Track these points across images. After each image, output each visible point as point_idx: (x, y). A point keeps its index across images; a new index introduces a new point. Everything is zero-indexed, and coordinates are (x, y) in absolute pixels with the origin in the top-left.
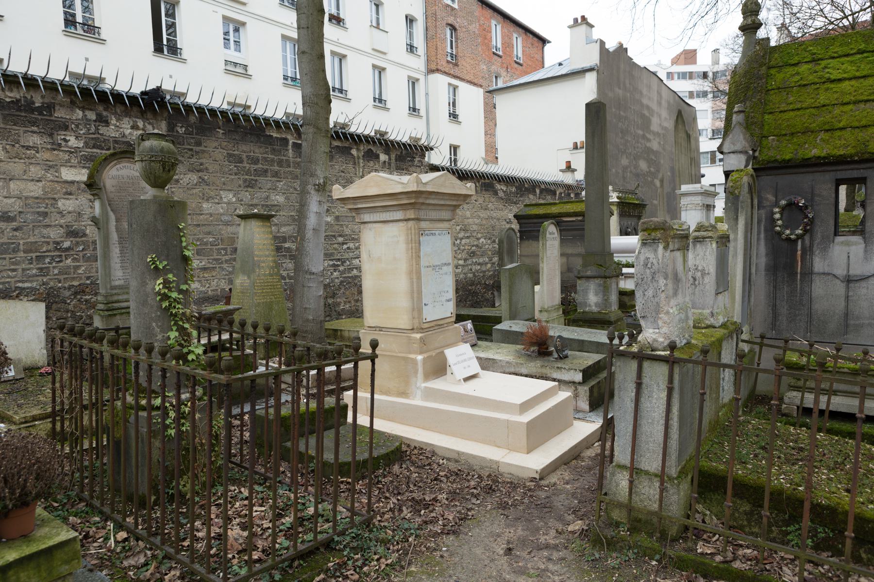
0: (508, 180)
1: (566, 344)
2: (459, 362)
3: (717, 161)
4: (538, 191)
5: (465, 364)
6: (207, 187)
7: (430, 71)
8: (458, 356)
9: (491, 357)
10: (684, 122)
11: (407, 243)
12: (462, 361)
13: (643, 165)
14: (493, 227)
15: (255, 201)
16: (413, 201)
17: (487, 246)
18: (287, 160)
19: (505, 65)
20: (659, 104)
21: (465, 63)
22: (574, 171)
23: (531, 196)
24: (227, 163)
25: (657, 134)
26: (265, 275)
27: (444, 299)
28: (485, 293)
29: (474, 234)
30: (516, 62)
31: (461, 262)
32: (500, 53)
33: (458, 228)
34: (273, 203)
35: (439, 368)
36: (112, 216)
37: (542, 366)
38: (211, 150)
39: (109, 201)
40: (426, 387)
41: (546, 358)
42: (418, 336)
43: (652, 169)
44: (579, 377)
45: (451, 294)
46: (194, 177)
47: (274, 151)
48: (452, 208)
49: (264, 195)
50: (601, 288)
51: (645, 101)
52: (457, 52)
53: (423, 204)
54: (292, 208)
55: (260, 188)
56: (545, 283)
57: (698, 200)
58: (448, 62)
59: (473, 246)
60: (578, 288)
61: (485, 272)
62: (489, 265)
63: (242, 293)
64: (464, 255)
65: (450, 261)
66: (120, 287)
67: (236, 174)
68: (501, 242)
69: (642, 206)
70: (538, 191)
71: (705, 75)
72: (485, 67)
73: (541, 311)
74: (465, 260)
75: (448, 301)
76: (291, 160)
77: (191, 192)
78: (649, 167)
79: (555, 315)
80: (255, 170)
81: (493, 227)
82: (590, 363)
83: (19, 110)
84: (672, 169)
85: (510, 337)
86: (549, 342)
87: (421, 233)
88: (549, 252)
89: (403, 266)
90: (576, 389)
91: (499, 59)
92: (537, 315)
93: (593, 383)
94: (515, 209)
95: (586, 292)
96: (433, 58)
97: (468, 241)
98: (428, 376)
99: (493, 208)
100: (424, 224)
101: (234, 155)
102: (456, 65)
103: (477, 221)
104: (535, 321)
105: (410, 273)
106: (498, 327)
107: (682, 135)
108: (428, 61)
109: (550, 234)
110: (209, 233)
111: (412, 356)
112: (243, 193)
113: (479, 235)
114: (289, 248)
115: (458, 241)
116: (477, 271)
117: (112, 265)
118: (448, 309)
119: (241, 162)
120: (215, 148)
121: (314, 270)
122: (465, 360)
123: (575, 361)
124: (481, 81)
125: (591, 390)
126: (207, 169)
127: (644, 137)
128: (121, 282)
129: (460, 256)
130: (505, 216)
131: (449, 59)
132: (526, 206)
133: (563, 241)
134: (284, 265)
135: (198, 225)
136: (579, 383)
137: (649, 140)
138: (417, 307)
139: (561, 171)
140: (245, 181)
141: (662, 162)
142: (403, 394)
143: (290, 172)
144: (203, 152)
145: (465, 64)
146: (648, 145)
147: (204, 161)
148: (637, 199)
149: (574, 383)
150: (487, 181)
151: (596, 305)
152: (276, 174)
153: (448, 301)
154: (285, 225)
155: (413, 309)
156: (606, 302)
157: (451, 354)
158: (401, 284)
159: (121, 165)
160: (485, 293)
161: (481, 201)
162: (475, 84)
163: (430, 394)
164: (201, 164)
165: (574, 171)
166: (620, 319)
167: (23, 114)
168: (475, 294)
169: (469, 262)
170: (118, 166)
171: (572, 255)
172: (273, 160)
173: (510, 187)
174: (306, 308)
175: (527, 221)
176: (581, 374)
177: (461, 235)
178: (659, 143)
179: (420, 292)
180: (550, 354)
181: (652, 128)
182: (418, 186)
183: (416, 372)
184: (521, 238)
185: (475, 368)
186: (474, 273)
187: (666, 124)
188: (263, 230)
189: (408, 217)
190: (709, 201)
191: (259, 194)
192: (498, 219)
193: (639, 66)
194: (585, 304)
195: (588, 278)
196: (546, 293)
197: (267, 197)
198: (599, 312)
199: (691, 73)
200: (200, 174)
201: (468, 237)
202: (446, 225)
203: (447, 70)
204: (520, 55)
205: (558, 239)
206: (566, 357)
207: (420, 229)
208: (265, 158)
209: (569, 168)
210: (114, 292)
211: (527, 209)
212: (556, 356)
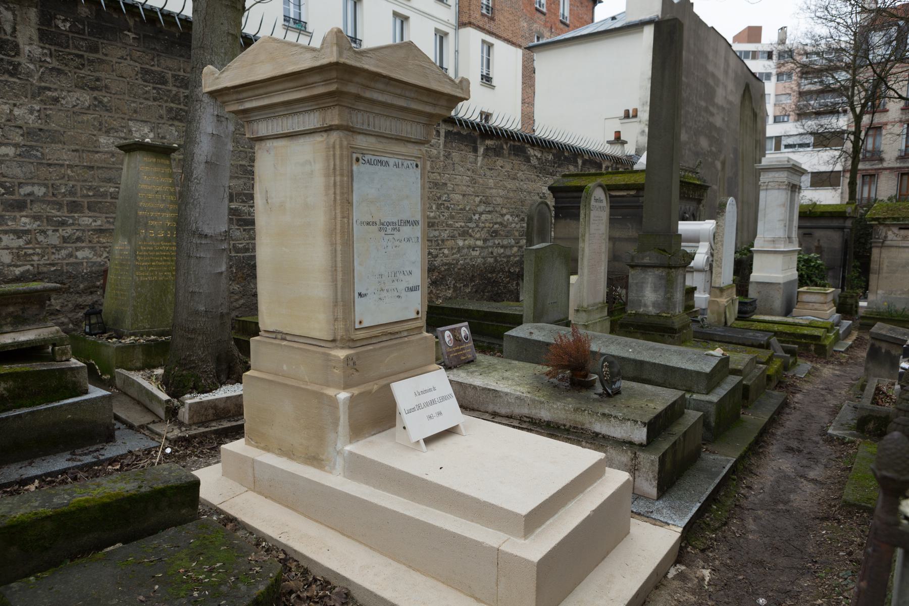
0: (546, 145)
1: (621, 369)
2: (419, 407)
3: (783, 147)
4: (580, 162)
5: (432, 410)
6: (107, 114)
7: (461, 24)
8: (418, 394)
9: (492, 385)
10: (751, 97)
11: (327, 176)
12: (427, 404)
13: (704, 143)
14: (523, 202)
16: (333, 87)
17: (513, 225)
19: (549, 24)
20: (726, 72)
21: (503, 18)
22: (624, 143)
23: (571, 168)
24: (140, 82)
25: (721, 108)
26: (156, 239)
27: (402, 286)
28: (509, 282)
29: (498, 209)
30: (562, 22)
31: (479, 243)
32: (544, 10)
33: (477, 199)
35: (380, 416)
37: (576, 410)
38: (115, 60)
40: (351, 453)
41: (584, 393)
42: (342, 354)
43: (714, 149)
44: (640, 435)
45: (417, 276)
46: (86, 98)
48: (424, 120)
50: (663, 282)
51: (710, 68)
52: (494, 4)
53: (358, 98)
54: (243, 155)
56: (586, 271)
57: (783, 176)
58: (483, 15)
59: (496, 223)
60: (630, 280)
61: (509, 257)
62: (515, 249)
63: (121, 265)
64: (484, 234)
65: (418, 217)
67: (155, 100)
68: (530, 218)
69: (703, 188)
70: (580, 162)
71: (770, 55)
72: (525, 24)
73: (577, 311)
74: (485, 240)
75: (412, 289)
77: (80, 119)
78: (710, 146)
79: (597, 316)
81: (523, 202)
82: (660, 408)
84: (735, 151)
85: (530, 351)
86: (590, 366)
87: (355, 156)
88: (593, 227)
89: (320, 219)
90: (635, 457)
91: (543, 17)
92: (572, 317)
93: (665, 446)
94: (550, 182)
95: (641, 286)
96: (466, 10)
97: (489, 216)
98: (358, 431)
99: (523, 178)
100: (361, 141)
101: (152, 72)
102: (492, 19)
103: (502, 192)
104: (568, 324)
105: (331, 232)
106: (513, 332)
107: (748, 113)
108: (460, 13)
109: (596, 200)
110: (109, 180)
111: (330, 392)
112: (166, 127)
113: (504, 211)
115: (477, 217)
116: (500, 255)
118: (412, 306)
119: (165, 83)
120: (122, 58)
121: (207, 230)
122: (433, 402)
123: (633, 403)
124: (520, 41)
125: (662, 461)
126: (106, 87)
127: (706, 110)
129: (478, 236)
130: (539, 189)
131: (484, 11)
132: (565, 176)
133: (612, 221)
135: (91, 168)
136: (641, 445)
137: (712, 114)
138: (344, 298)
139: (609, 142)
140: (170, 110)
141: (725, 141)
142: (315, 460)
144: (102, 61)
145: (502, 18)
146: (711, 119)
147: (102, 75)
148: (698, 179)
149: (631, 443)
150: (517, 143)
151: (655, 304)
153: (412, 289)
155: (335, 304)
156: (668, 301)
157: (404, 392)
158: (315, 254)
160: (509, 282)
161: (508, 167)
162: (513, 44)
163: (361, 469)
164: (98, 79)
165: (624, 143)
166: (686, 326)
168: (495, 283)
169: (490, 243)
171: (620, 239)
173: (546, 154)
174: (193, 293)
175: (564, 195)
176: (645, 430)
177: (481, 208)
178: (723, 119)
179: (349, 271)
180: (590, 385)
181: (716, 101)
182: (340, 53)
183: (336, 423)
184: (557, 217)
185: (452, 414)
186: (495, 258)
187: (731, 98)
188: (155, 169)
189: (329, 122)
190: (794, 180)
192: (530, 193)
193: (706, 25)
194: (639, 303)
195: (645, 267)
196: (587, 286)
198: (658, 316)
199: (754, 53)
200: (96, 93)
201: (490, 212)
202: (413, 150)
203: (481, 24)
204: (567, 14)
205: (608, 210)
206: (618, 392)
207: (353, 149)
209: (618, 139)
211: (565, 180)
212: (600, 390)
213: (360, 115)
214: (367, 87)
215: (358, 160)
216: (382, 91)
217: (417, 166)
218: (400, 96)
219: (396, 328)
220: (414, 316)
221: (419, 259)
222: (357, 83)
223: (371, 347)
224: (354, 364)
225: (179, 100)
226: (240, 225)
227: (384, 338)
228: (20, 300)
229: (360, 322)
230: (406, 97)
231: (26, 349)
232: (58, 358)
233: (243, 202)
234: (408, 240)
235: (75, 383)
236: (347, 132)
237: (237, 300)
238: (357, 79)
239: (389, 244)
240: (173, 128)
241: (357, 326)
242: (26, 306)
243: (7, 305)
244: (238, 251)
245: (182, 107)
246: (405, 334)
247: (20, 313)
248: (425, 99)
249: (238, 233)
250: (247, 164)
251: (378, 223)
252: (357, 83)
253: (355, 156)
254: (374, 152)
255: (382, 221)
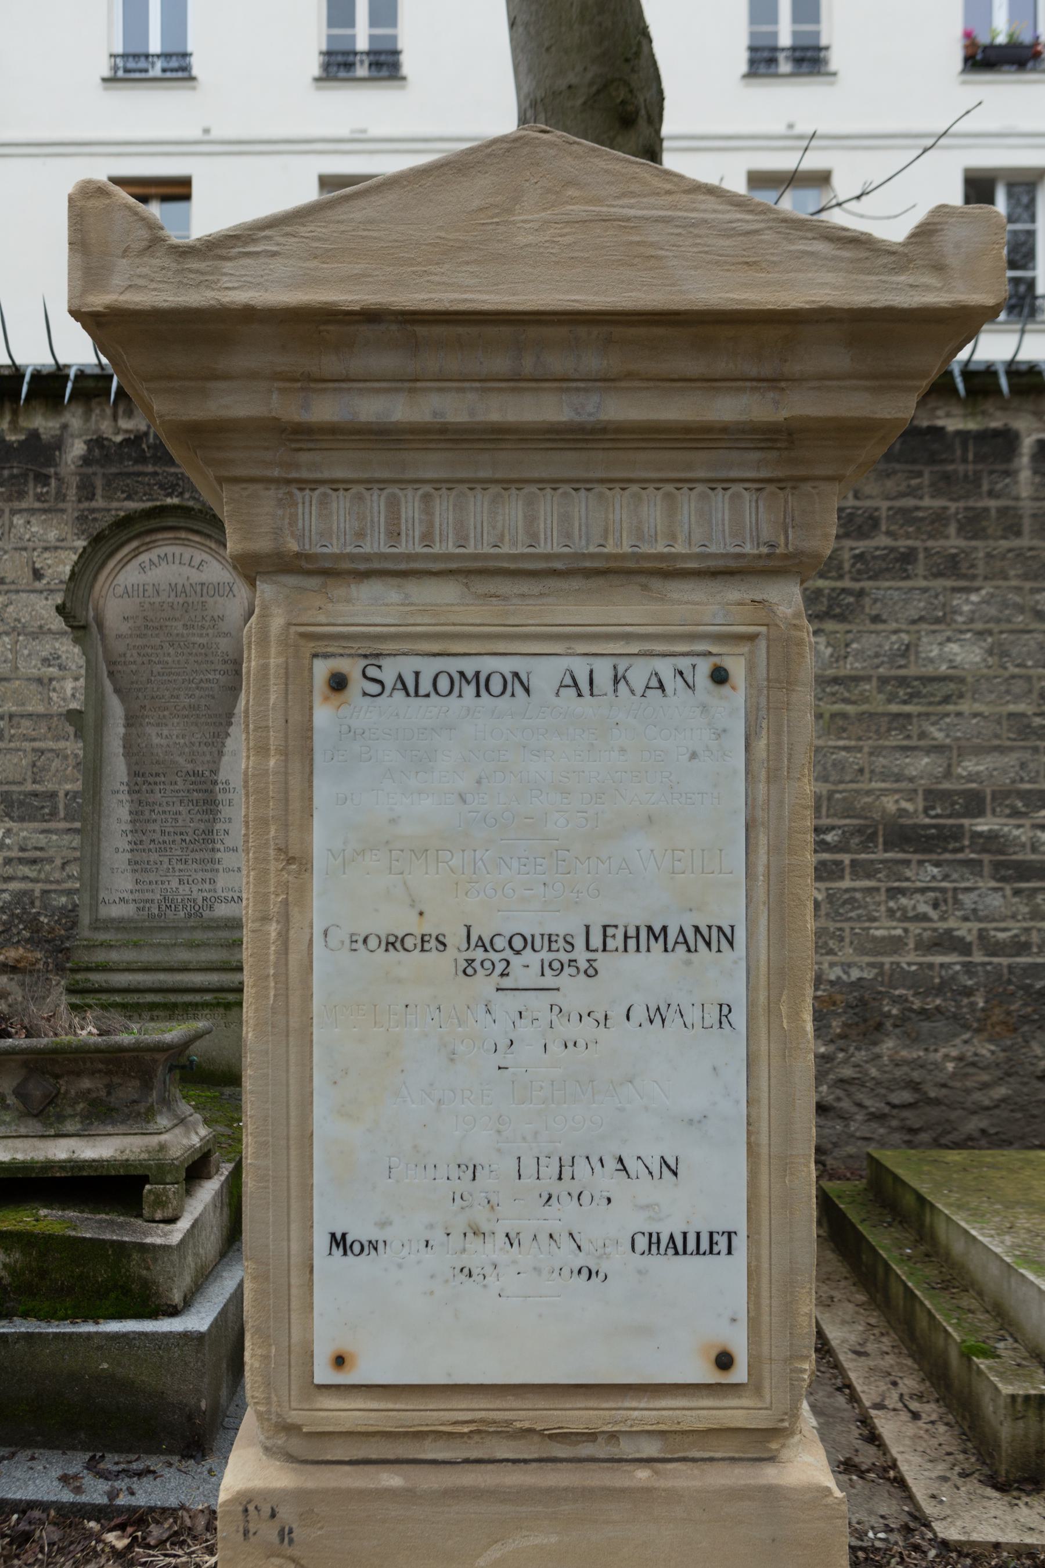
15: (850, 667)
18: (1003, 511)
34: (929, 670)
36: (116, 708)
39: (110, 663)
47: (945, 484)
48: (749, 464)
49: (892, 643)
55: (876, 619)
65: (730, 909)
66: (120, 925)
76: (1027, 507)
80: (860, 557)
83: (142, 459)
114: (992, 837)
117: (106, 855)
128: (126, 911)
134: (967, 899)
143: (1020, 554)
152: (951, 566)
154: (979, 751)
159: (153, 555)
167: (150, 469)
170: (144, 557)
172: (940, 518)
191: (869, 642)
197: (906, 651)
208: (904, 511)
210: (102, 936)
213: (341, 504)
214: (310, 382)
215: (338, 683)
216: (408, 383)
217: (719, 677)
218: (516, 382)
219: (576, 1416)
220: (705, 1373)
221: (734, 1107)
222: (253, 375)
223: (392, 1479)
224: (285, 1535)
225: (840, 567)
226: (1003, 879)
227: (504, 1450)
228: (101, 1066)
229: (340, 1361)
230: (563, 382)
231: (89, 1178)
232: (146, 1212)
233: (1015, 813)
234: (657, 1015)
235: (145, 1284)
236: (292, 580)
237: (985, 1086)
238: (241, 361)
239: (525, 1029)
240: (822, 640)
241: (324, 1374)
242: (116, 1080)
243: (78, 1074)
244: (994, 949)
245: (847, 583)
246: (651, 1449)
247: (103, 1093)
248: (692, 366)
249: (996, 901)
250: (1030, 710)
251: (455, 938)
252: (253, 375)
253: (322, 670)
254: (442, 641)
255: (483, 930)
